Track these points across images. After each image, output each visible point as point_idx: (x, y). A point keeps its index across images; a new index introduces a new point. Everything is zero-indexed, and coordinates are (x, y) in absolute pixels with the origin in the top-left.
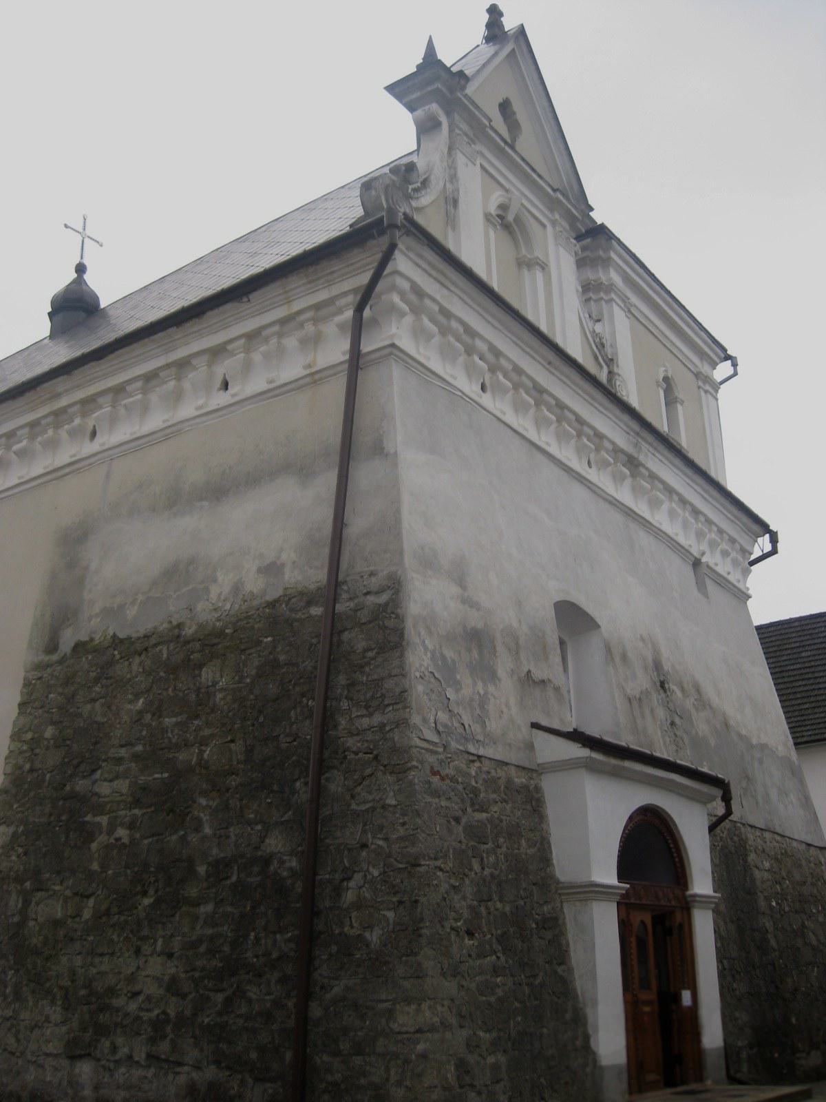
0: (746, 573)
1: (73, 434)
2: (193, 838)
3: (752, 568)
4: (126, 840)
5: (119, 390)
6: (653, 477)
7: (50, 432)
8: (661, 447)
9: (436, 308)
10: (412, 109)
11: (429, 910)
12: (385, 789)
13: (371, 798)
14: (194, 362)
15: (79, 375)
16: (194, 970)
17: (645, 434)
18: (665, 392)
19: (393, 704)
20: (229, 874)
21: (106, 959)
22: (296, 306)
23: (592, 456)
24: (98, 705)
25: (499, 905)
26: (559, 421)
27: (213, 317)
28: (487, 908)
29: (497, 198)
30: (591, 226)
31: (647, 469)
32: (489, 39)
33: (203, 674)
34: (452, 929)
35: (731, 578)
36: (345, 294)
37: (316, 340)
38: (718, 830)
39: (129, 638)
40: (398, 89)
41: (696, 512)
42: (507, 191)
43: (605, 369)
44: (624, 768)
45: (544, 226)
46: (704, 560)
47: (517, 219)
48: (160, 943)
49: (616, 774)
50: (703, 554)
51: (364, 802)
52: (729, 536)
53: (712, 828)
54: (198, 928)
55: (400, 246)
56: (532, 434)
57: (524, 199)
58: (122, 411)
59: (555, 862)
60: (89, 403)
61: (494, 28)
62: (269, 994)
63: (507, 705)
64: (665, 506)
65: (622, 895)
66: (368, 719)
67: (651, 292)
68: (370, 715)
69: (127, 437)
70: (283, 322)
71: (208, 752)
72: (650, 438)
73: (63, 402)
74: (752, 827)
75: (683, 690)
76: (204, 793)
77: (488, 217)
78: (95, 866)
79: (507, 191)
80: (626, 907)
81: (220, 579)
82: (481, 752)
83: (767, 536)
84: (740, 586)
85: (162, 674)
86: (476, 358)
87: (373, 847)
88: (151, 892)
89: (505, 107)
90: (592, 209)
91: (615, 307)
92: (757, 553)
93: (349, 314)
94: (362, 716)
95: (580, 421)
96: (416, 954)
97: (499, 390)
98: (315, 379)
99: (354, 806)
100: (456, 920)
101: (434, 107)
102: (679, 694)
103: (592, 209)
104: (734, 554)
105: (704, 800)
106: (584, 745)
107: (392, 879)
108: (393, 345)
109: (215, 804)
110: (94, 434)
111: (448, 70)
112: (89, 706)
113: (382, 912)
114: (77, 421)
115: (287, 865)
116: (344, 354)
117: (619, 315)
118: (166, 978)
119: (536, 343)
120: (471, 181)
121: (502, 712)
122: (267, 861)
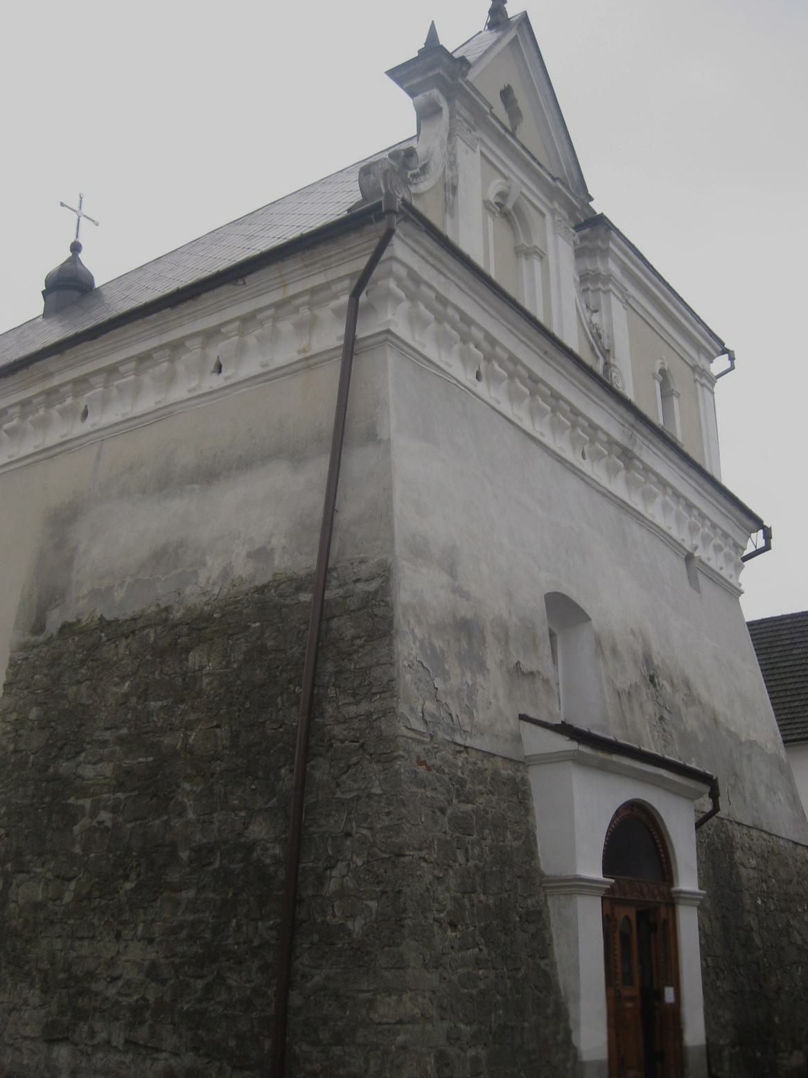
0: (739, 568)
1: (64, 413)
2: (177, 823)
3: (745, 563)
4: (109, 824)
5: (112, 371)
6: (647, 470)
7: (42, 412)
8: (656, 440)
9: (433, 295)
10: (412, 93)
11: (412, 901)
12: (371, 777)
13: (356, 786)
14: (188, 344)
15: (71, 355)
16: (174, 955)
17: (639, 426)
18: (662, 384)
19: (380, 693)
20: (212, 860)
21: (86, 943)
22: (292, 290)
23: (586, 448)
24: (83, 687)
25: (483, 897)
26: (553, 411)
27: (208, 299)
28: (470, 900)
29: (496, 185)
30: (590, 216)
31: (641, 462)
32: (492, 25)
33: (190, 658)
34: (435, 920)
35: (724, 573)
36: (341, 279)
37: (309, 326)
38: (705, 827)
39: (116, 620)
40: (399, 74)
41: (690, 506)
42: (506, 178)
43: (602, 361)
44: (613, 763)
45: (543, 215)
46: (696, 554)
47: (516, 207)
48: (140, 927)
49: (603, 768)
50: (696, 548)
51: (350, 791)
52: (723, 530)
53: (699, 825)
54: (179, 914)
55: (398, 231)
56: (527, 424)
57: (524, 187)
58: (115, 392)
59: (540, 855)
60: (81, 383)
61: (497, 18)
62: (249, 982)
63: (495, 696)
64: (659, 500)
65: (607, 890)
66: (355, 707)
67: (632, 266)
68: (357, 703)
69: (120, 418)
70: (278, 305)
71: (193, 737)
72: (645, 431)
73: (56, 381)
74: (739, 824)
75: (672, 685)
76: (188, 778)
77: (486, 204)
78: (77, 850)
79: (506, 178)
80: (611, 901)
81: (209, 563)
82: (468, 743)
83: (761, 532)
84: (732, 581)
85: (149, 657)
86: (472, 346)
87: (357, 836)
88: (133, 876)
89: (506, 94)
90: (591, 199)
91: (613, 298)
92: (750, 549)
93: (345, 299)
94: (349, 704)
95: (575, 412)
96: (398, 945)
97: (494, 379)
98: (309, 363)
99: (339, 795)
100: (440, 911)
101: (435, 93)
102: (668, 688)
103: (591, 199)
104: (726, 549)
105: (691, 796)
106: (572, 738)
107: (376, 868)
108: (388, 332)
109: (200, 789)
110: (85, 414)
111: (450, 55)
112: (74, 688)
113: (365, 902)
114: (69, 401)
115: (271, 852)
116: (339, 339)
117: (617, 306)
118: (146, 963)
119: (532, 332)
120: (470, 167)
121: (490, 703)
122: (250, 848)
